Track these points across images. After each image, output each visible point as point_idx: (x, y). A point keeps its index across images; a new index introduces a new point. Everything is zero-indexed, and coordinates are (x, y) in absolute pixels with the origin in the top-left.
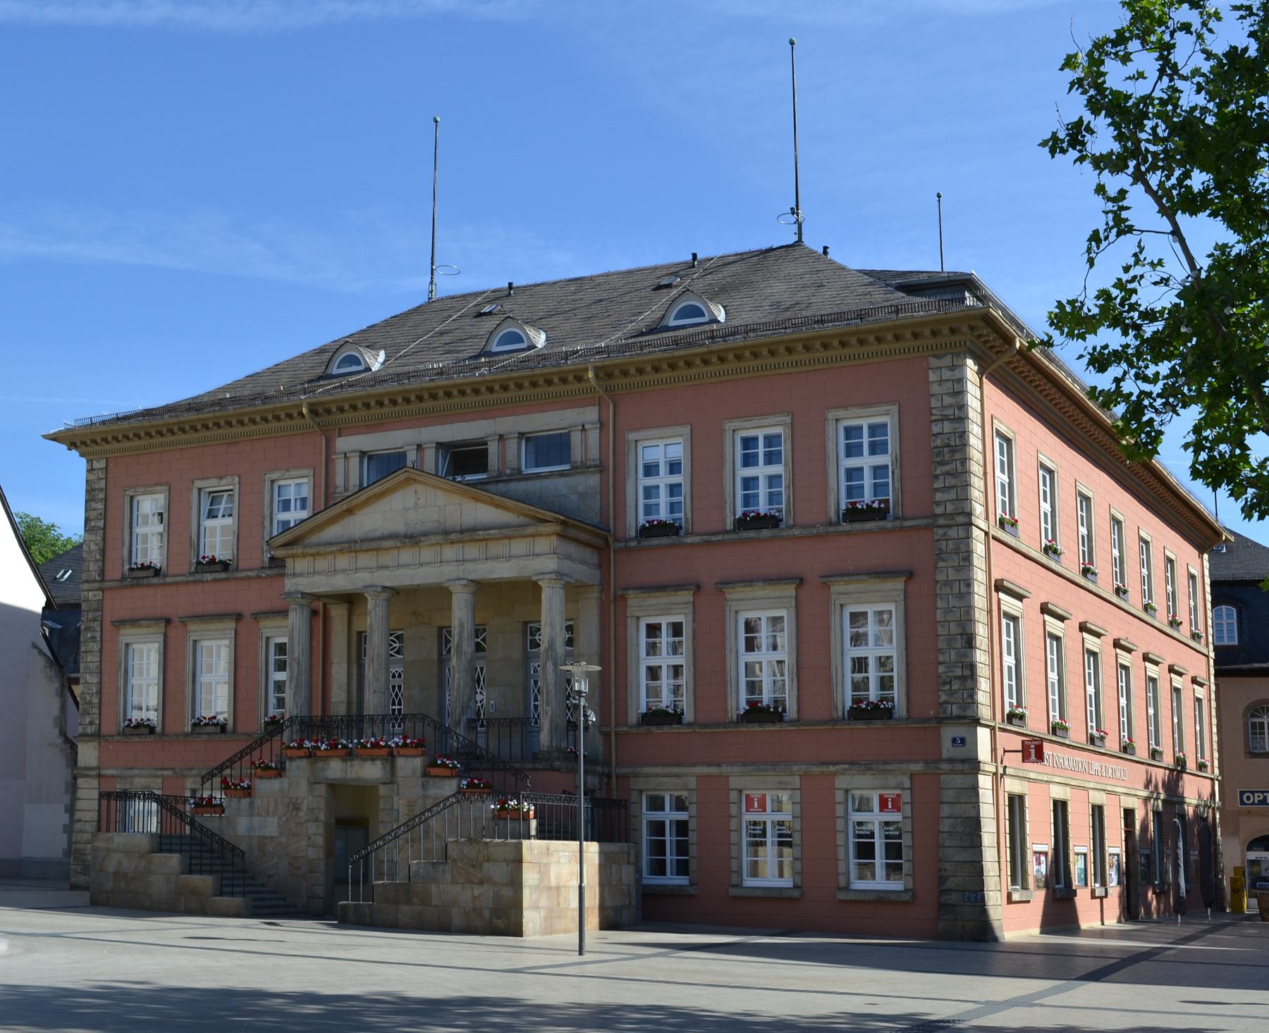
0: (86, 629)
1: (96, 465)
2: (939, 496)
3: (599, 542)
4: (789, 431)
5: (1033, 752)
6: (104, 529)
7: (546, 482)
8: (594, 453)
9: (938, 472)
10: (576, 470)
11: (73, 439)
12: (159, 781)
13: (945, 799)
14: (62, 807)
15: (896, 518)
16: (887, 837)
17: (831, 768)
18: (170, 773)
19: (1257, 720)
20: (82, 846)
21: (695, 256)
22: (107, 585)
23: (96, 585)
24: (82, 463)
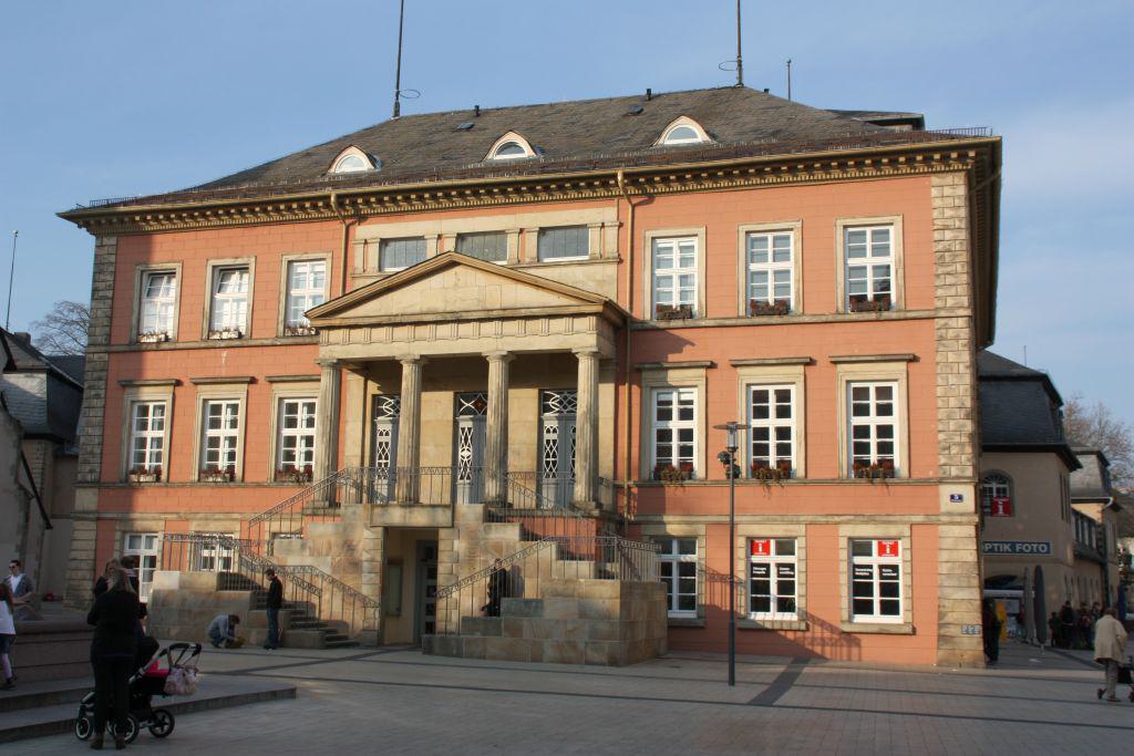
0: (89, 388)
1: (106, 241)
2: (940, 292)
5: (1001, 508)
6: (112, 299)
7: (564, 270)
9: (940, 271)
10: (593, 262)
11: (79, 217)
12: (162, 523)
13: (944, 546)
14: (14, 548)
15: (899, 311)
16: (779, 576)
17: (837, 519)
18: (175, 516)
19: (987, 486)
20: (76, 583)
21: (649, 91)
22: (113, 349)
23: (103, 349)
24: (91, 240)
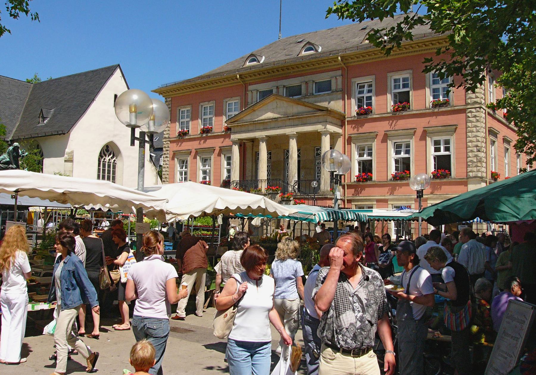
1: (168, 100)
4: (412, 76)
8: (340, 86)
24: (163, 99)
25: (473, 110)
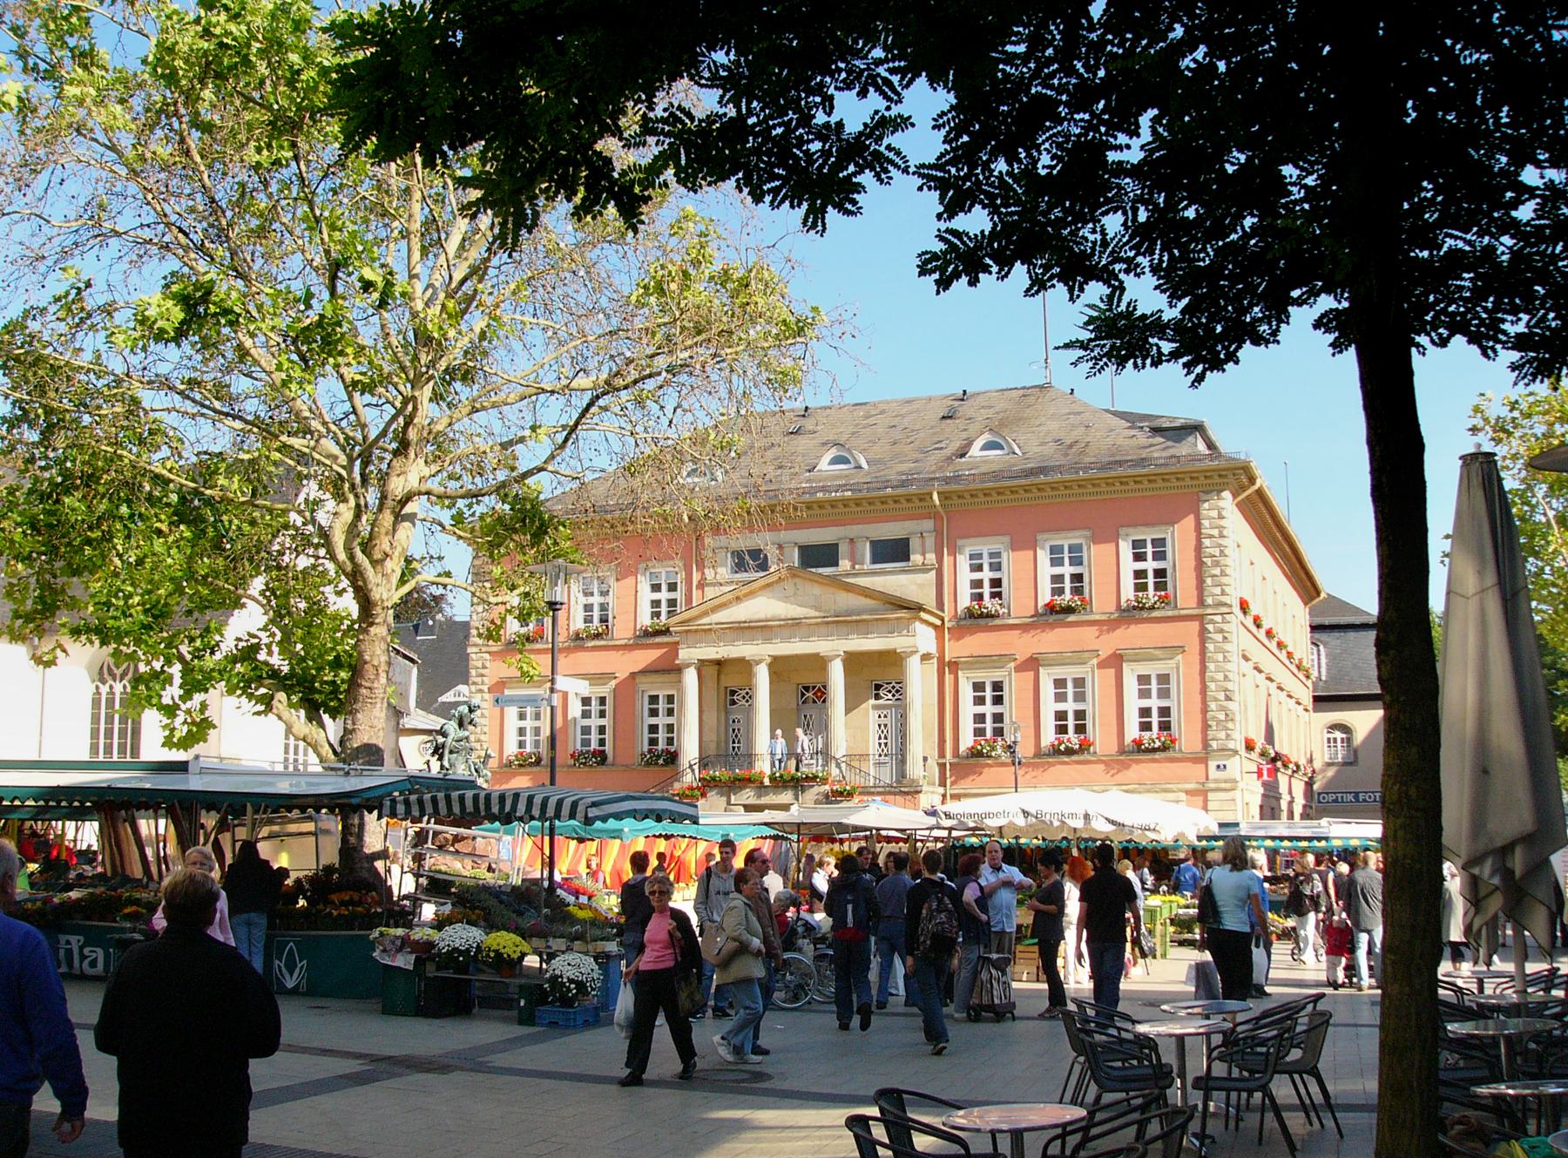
3: (938, 622)
25: (1218, 618)
